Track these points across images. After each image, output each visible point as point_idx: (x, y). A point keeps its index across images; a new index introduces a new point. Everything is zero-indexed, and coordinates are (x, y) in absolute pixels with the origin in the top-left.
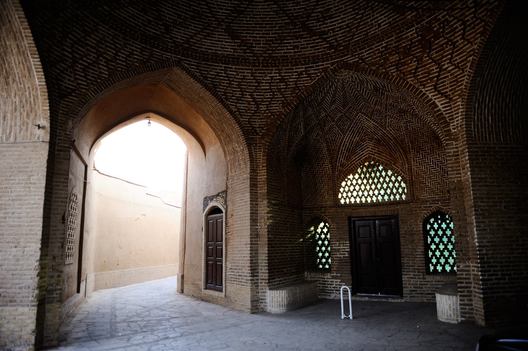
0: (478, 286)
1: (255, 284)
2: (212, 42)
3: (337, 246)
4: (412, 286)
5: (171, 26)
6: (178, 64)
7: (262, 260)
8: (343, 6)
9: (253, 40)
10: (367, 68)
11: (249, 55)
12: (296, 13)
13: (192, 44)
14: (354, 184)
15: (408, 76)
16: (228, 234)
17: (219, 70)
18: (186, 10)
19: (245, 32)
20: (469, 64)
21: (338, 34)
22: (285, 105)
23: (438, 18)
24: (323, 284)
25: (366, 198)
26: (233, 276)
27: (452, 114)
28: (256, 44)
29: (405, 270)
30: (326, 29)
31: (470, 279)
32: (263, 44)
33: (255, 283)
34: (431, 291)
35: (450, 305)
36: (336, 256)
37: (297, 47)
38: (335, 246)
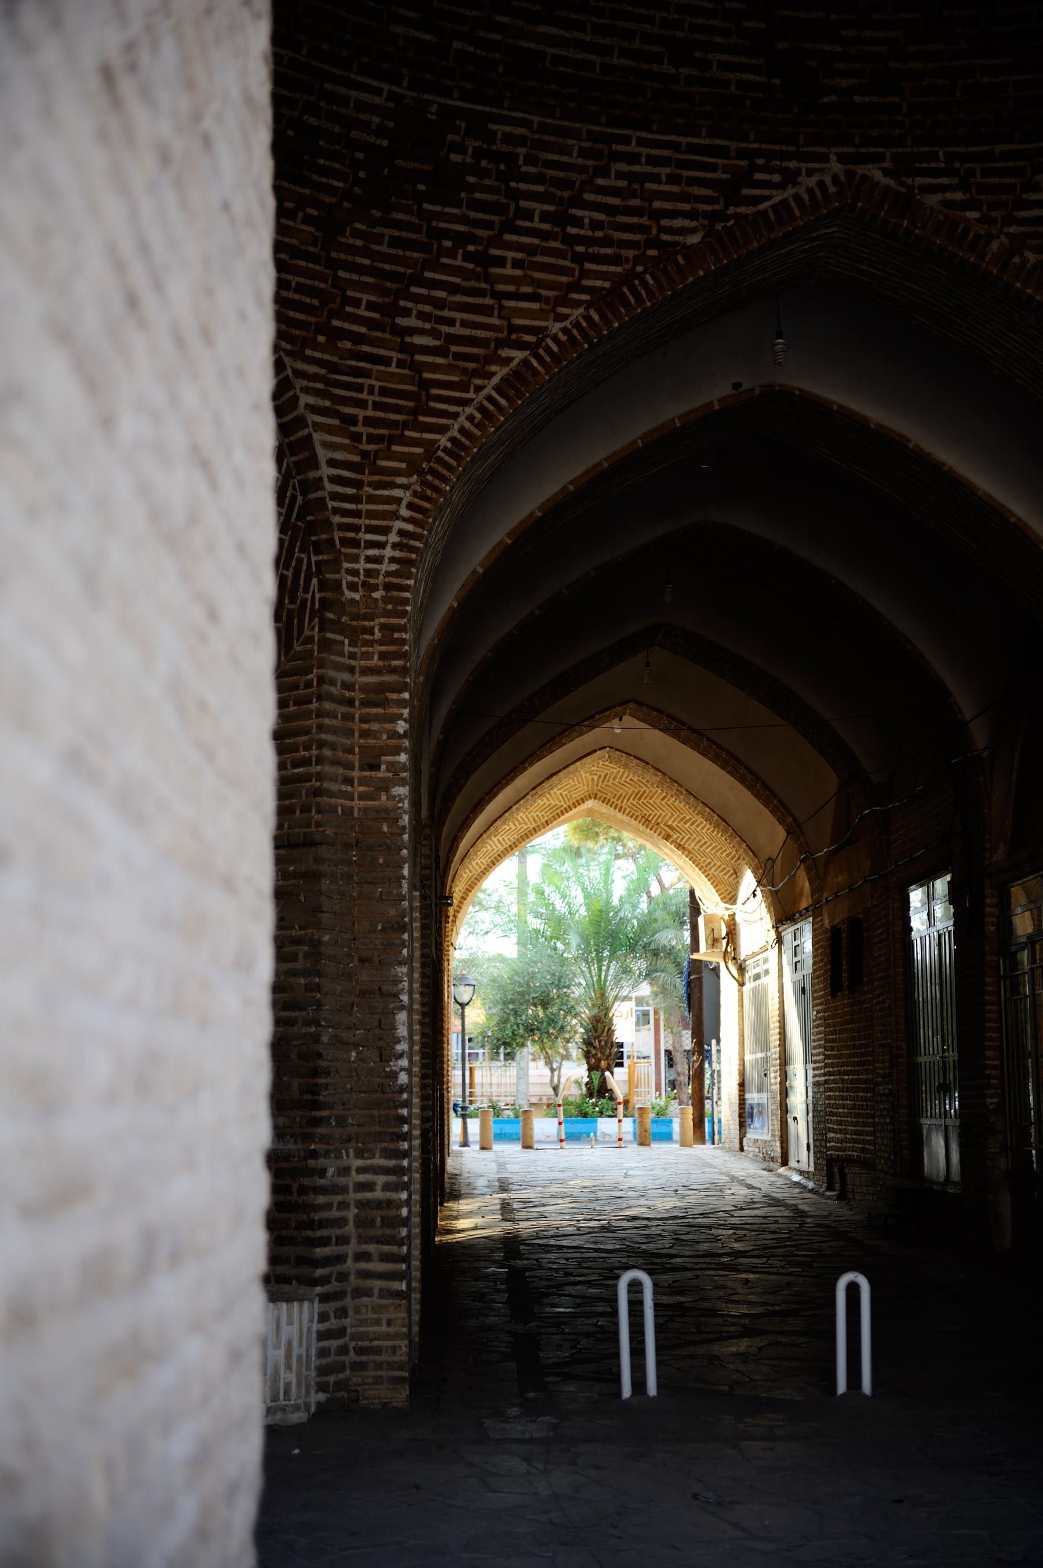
20: (500, 372)
23: (492, 126)
27: (356, 521)
31: (344, 1221)
35: (290, 1343)
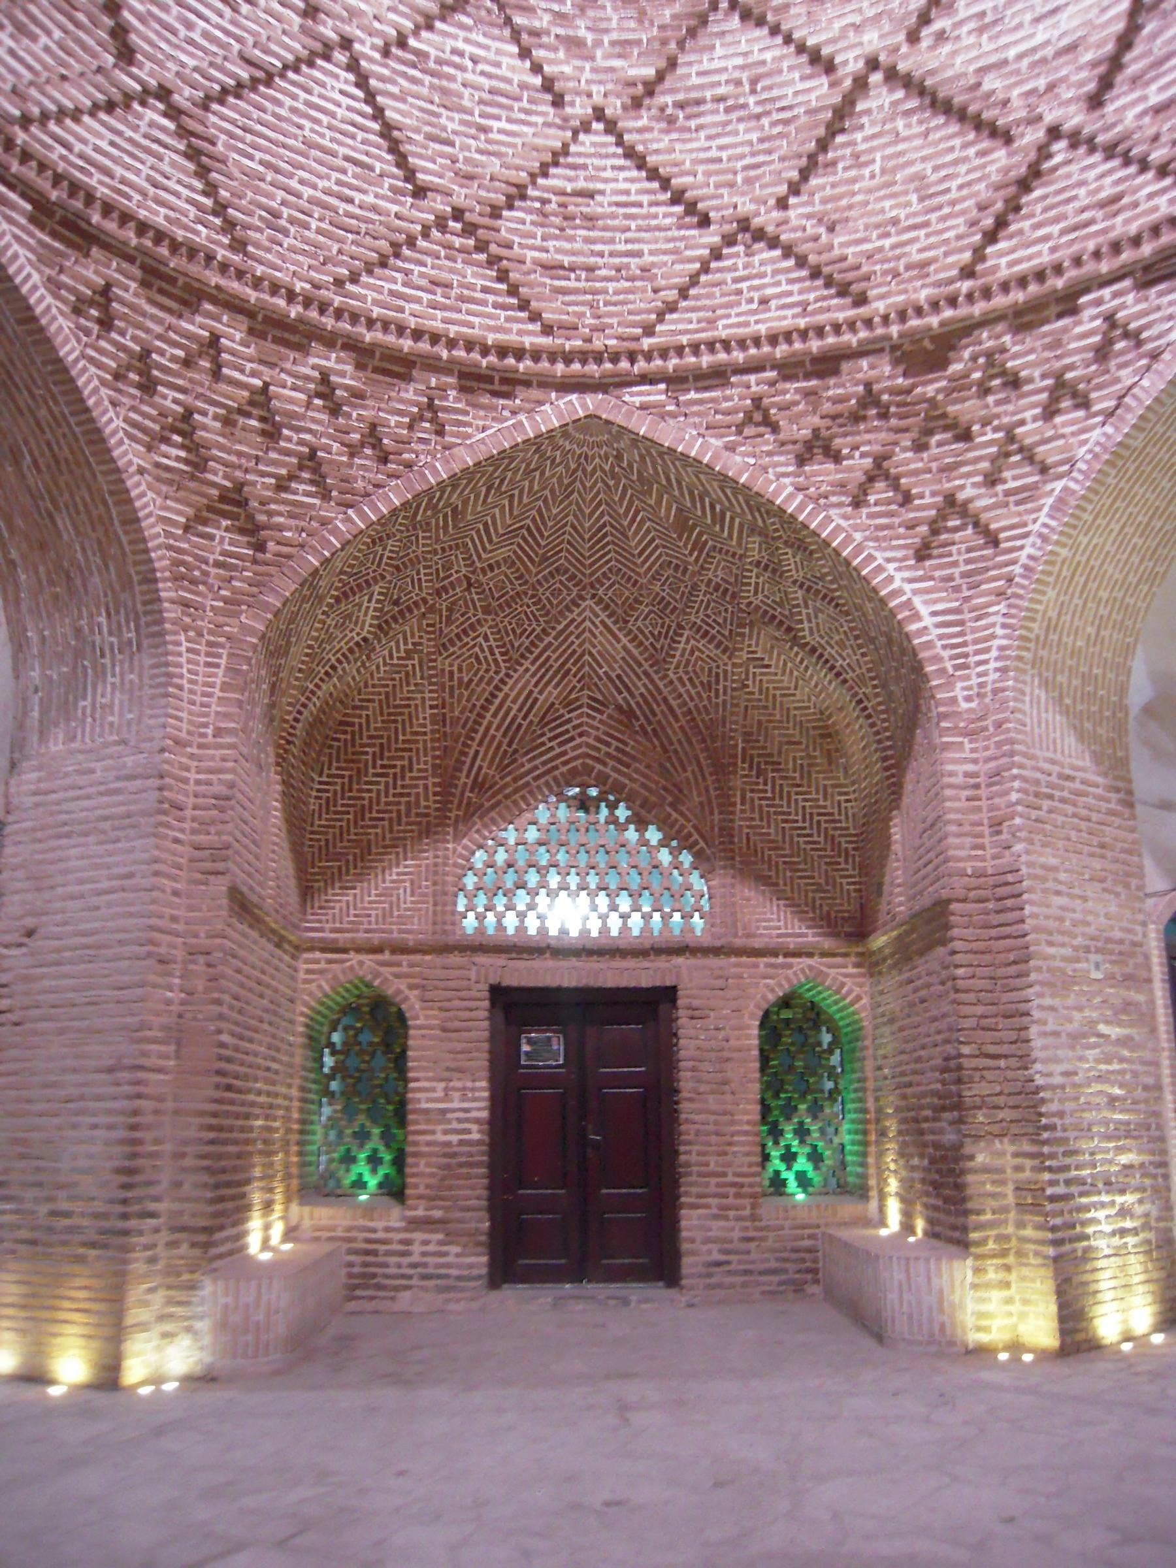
2: (118, 140)
4: (714, 1247)
19: (258, 155)
28: (292, 221)
29: (694, 1190)
32: (319, 231)
34: (778, 1260)
36: (428, 1138)
38: (429, 1100)
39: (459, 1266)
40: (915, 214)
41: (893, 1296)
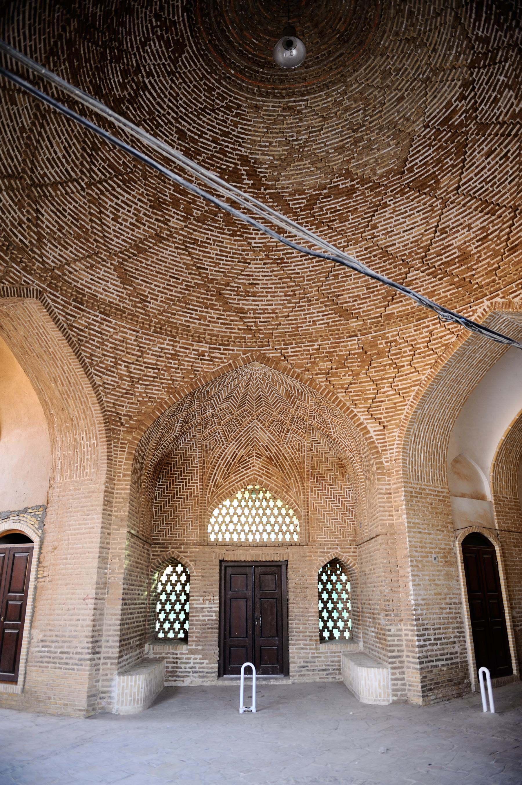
0: (414, 655)
1: (95, 667)
3: (200, 604)
4: (302, 660)
5: (45, 238)
6: (39, 295)
7: (110, 625)
8: (273, 286)
9: (149, 293)
10: (290, 369)
11: (140, 311)
12: (211, 275)
13: (67, 272)
14: (232, 514)
15: (339, 390)
16: (41, 580)
17: (93, 320)
18: (72, 222)
19: (140, 278)
20: (413, 394)
21: (260, 318)
22: (172, 391)
24: (174, 663)
25: (246, 534)
26: (46, 654)
28: (152, 298)
29: (294, 638)
30: (246, 307)
31: (402, 645)
32: (161, 301)
33: (95, 665)
35: (379, 681)
37: (205, 318)
39: (207, 668)
40: (365, 294)
41: (363, 682)
